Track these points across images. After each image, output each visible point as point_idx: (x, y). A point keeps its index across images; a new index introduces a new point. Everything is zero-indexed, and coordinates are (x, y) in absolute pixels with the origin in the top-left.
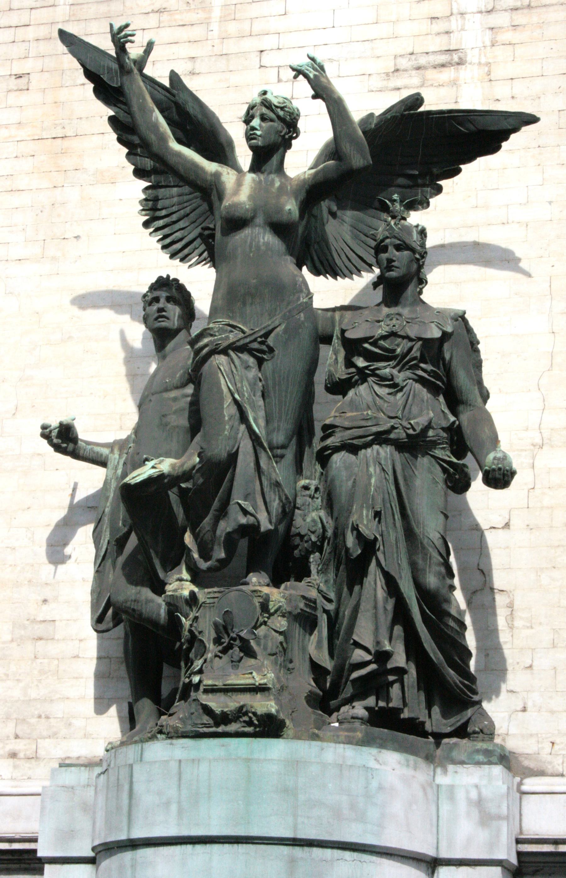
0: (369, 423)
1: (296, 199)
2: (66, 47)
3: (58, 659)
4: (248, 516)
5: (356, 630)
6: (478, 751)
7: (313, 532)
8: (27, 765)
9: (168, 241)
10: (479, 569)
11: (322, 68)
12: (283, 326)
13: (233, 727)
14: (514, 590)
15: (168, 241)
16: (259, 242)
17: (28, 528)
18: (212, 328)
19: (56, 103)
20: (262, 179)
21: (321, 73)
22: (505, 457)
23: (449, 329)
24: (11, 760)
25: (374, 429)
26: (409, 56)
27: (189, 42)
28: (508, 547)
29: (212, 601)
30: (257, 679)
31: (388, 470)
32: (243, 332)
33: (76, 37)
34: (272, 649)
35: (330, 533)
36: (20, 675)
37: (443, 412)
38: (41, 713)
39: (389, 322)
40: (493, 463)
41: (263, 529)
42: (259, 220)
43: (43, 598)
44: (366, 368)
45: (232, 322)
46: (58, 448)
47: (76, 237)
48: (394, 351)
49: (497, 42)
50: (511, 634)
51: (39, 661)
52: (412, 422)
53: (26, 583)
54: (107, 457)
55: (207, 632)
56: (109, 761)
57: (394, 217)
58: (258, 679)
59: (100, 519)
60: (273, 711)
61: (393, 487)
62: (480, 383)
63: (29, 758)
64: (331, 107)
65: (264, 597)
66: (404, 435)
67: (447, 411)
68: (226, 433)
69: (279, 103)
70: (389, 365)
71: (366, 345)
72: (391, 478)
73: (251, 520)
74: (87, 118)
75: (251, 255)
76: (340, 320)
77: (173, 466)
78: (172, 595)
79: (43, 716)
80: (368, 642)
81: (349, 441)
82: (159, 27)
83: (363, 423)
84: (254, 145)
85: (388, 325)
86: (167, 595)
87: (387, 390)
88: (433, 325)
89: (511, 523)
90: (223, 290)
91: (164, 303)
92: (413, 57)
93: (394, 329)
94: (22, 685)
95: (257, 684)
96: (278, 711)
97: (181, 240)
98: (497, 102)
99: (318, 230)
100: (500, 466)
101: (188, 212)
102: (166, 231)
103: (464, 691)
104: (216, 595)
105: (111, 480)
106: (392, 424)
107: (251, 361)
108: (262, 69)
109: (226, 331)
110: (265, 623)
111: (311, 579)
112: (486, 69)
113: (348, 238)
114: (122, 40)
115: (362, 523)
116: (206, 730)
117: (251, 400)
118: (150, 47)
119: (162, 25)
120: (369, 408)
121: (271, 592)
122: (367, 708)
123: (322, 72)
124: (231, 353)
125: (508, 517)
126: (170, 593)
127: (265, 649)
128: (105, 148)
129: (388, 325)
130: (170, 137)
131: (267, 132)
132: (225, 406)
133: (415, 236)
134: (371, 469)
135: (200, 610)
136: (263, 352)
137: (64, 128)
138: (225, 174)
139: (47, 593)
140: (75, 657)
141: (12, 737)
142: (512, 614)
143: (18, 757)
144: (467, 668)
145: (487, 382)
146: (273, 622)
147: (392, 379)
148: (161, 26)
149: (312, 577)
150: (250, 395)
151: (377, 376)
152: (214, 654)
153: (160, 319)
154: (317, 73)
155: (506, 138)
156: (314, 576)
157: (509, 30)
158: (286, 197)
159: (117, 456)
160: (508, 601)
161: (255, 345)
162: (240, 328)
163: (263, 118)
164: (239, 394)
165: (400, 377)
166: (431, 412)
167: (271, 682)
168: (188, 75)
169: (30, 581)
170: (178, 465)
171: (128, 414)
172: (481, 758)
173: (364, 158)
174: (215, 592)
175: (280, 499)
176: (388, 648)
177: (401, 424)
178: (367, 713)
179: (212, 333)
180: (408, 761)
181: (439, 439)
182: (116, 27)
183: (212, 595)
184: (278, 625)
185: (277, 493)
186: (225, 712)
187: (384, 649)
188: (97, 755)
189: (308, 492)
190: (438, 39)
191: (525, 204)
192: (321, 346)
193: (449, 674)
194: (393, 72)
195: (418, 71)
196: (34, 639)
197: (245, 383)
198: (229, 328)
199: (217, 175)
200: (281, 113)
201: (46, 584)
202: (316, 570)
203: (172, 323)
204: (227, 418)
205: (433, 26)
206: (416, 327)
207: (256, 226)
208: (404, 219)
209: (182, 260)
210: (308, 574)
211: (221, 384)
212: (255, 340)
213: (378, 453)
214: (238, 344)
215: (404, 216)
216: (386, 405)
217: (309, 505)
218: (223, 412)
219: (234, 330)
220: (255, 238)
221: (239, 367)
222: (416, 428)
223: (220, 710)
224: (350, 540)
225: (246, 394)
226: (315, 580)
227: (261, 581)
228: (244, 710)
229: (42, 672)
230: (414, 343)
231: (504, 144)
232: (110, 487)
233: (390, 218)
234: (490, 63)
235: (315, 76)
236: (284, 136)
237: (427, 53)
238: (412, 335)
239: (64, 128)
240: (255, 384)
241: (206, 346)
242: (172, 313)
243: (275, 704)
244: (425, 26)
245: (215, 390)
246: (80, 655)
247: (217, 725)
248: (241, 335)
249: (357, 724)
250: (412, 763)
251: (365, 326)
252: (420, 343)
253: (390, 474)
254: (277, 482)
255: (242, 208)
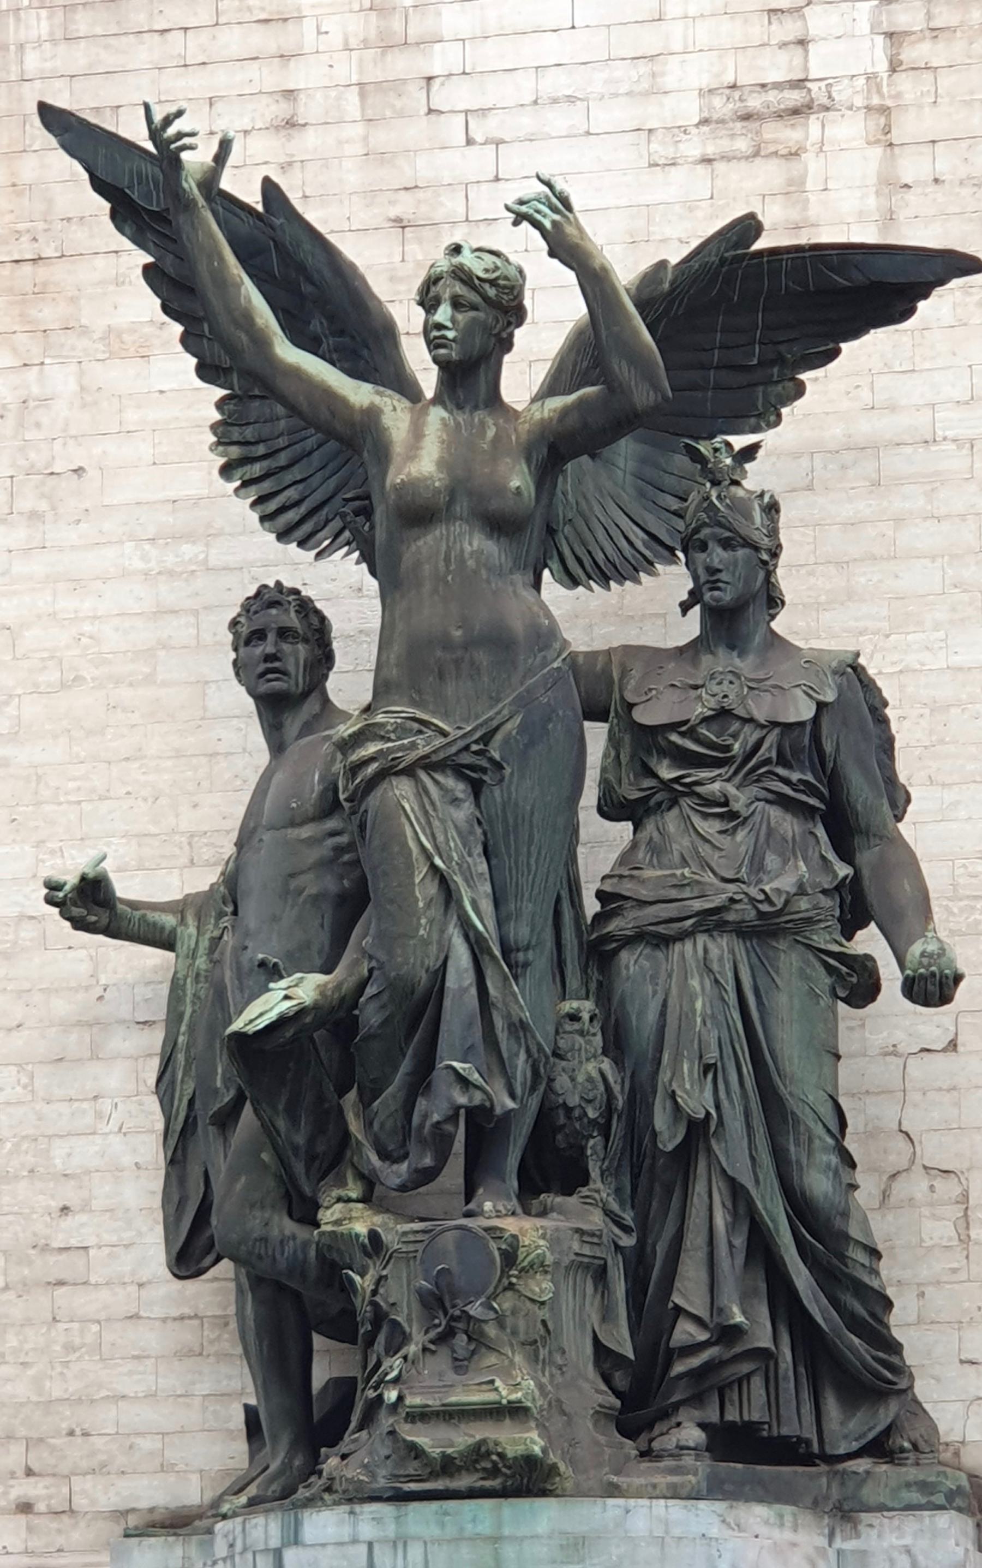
0: (687, 893)
1: (528, 461)
2: (56, 136)
3: (99, 1322)
4: (472, 1090)
5: (677, 1284)
6: (908, 1485)
7: (589, 1101)
8: (54, 1525)
9: (272, 506)
10: (901, 1131)
11: (565, 202)
12: (518, 720)
13: (463, 1482)
14: (968, 1170)
15: (272, 506)
16: (462, 551)
17: (20, 1065)
18: (382, 725)
19: (14, 185)
20: (460, 420)
21: (564, 216)
22: (942, 951)
23: (829, 696)
24: (22, 1519)
25: (697, 905)
26: (727, 91)
27: (282, 56)
28: (954, 1088)
29: (411, 1248)
30: (504, 1393)
31: (727, 982)
32: (444, 734)
33: (73, 115)
34: (527, 1333)
35: (620, 1102)
36: (27, 1354)
37: (823, 858)
38: (74, 1426)
39: (716, 689)
40: (920, 963)
41: (498, 1111)
42: (462, 506)
43: (61, 1205)
44: (677, 780)
45: (420, 715)
46: (79, 924)
47: (75, 471)
48: (728, 748)
49: (901, 63)
50: (965, 1253)
51: (61, 1326)
52: (767, 888)
53: (25, 1173)
54: (173, 931)
55: (405, 1304)
56: (231, 1538)
57: (715, 483)
58: (505, 1393)
59: (169, 1059)
60: (537, 1450)
61: (736, 1015)
62: (891, 780)
63: (56, 1513)
64: (588, 290)
65: (509, 1240)
66: (753, 913)
67: (831, 856)
68: (422, 932)
69: (487, 271)
70: (719, 775)
71: (674, 738)
72: (732, 998)
73: (478, 1098)
74: (82, 218)
75: (450, 578)
76: (621, 680)
77: (322, 989)
78: (333, 1232)
79: (78, 1432)
80: (699, 1307)
81: (651, 928)
82: (217, 24)
83: (674, 894)
84: (443, 359)
85: (714, 696)
86: (323, 1233)
87: (717, 825)
88: (798, 692)
89: (960, 1040)
90: (397, 649)
91: (276, 644)
92: (737, 95)
93: (726, 703)
94: (31, 1372)
95: (504, 1402)
96: (544, 1451)
97: (297, 504)
98: (905, 189)
99: (570, 497)
100: (933, 968)
101: (308, 449)
102: (266, 487)
103: (879, 1372)
104: (419, 1237)
105: (185, 980)
106: (730, 895)
107: (459, 788)
108: (433, 117)
109: (411, 730)
110: (511, 1286)
111: (590, 1190)
112: (882, 120)
113: (627, 498)
114: (173, 146)
115: (682, 1086)
116: (413, 1486)
117: (465, 865)
118: (225, 146)
119: (222, 20)
120: (684, 862)
121: (521, 1229)
122: (702, 1426)
123: (567, 213)
124: (423, 775)
125: (953, 1029)
126: (329, 1228)
127: (514, 1333)
128: (123, 283)
129: (714, 696)
130: (275, 334)
131: (467, 332)
132: (417, 880)
133: (757, 515)
134: (695, 983)
135: (390, 1266)
136: (484, 770)
137: (35, 239)
138: (387, 409)
139: (69, 1195)
140: (131, 1317)
141: (20, 1472)
142: (966, 1215)
143: (36, 1510)
144: (885, 1331)
145: (904, 769)
146: (526, 1285)
147: (726, 804)
148: (222, 20)
149: (592, 1186)
150: (462, 857)
151: (699, 795)
152: (420, 1346)
153: (270, 676)
154: (557, 217)
155: (926, 296)
156: (595, 1182)
157: (924, 38)
158: (508, 460)
159: (192, 930)
160: (958, 1190)
161: (466, 759)
162: (436, 726)
163: (457, 304)
164: (441, 858)
165: (740, 799)
166: (801, 863)
167: (530, 1397)
168: (283, 127)
169: (32, 1171)
170: (330, 986)
171: (205, 833)
172: (915, 1497)
173: (656, 387)
174: (417, 1232)
175: (528, 1051)
176: (739, 1318)
177: (745, 893)
178: (703, 1435)
179: (382, 733)
180: (781, 1516)
181: (818, 914)
182: (158, 118)
183: (411, 1238)
184: (537, 1289)
185: (523, 1041)
186: (449, 1456)
187: (732, 1322)
188: (188, 1502)
189: (576, 1026)
190: (783, 57)
191: (967, 403)
192: (587, 724)
193: (851, 1348)
194: (697, 125)
195: (745, 124)
196: (49, 1283)
197: (452, 832)
198: (416, 726)
199: (372, 413)
200: (492, 292)
201: (65, 1175)
202: (598, 1171)
203: (292, 682)
204: (421, 904)
205: (774, 27)
206: (767, 697)
207: (456, 519)
208: (736, 483)
209: (301, 544)
210: (585, 1180)
211: (406, 837)
212: (467, 748)
213: (706, 951)
214: (434, 758)
215: (735, 477)
216: (717, 854)
217: (580, 1050)
218: (414, 892)
219: (425, 730)
220: (455, 542)
221: (438, 803)
222: (774, 899)
223: (438, 1450)
224: (661, 1119)
225: (454, 854)
226: (598, 1191)
227: (501, 1208)
228: (483, 1449)
229: (69, 1348)
230: (765, 731)
231: (922, 305)
232: (185, 995)
233: (708, 485)
234: (889, 108)
235: (554, 223)
236: (499, 333)
237: (763, 86)
238: (761, 717)
239: (35, 239)
240: (472, 832)
241: (372, 759)
242: (292, 660)
243: (539, 1436)
244: (757, 29)
245: (396, 849)
246: (142, 1313)
247: (434, 1475)
248: (439, 741)
249: (688, 1460)
250: (788, 1519)
251: (671, 697)
252: (777, 731)
253: (729, 988)
254: (521, 1021)
255: (428, 487)
